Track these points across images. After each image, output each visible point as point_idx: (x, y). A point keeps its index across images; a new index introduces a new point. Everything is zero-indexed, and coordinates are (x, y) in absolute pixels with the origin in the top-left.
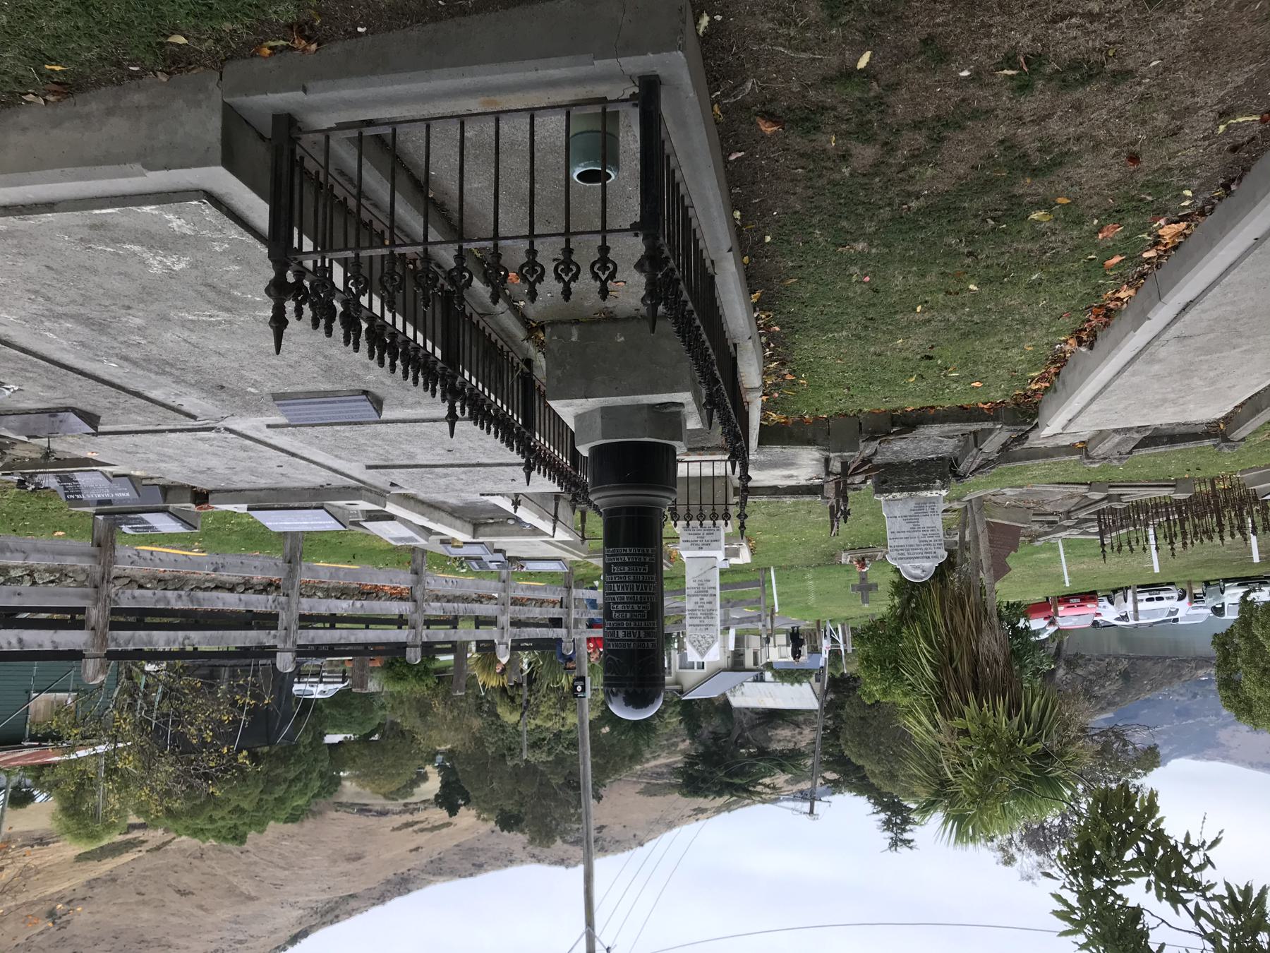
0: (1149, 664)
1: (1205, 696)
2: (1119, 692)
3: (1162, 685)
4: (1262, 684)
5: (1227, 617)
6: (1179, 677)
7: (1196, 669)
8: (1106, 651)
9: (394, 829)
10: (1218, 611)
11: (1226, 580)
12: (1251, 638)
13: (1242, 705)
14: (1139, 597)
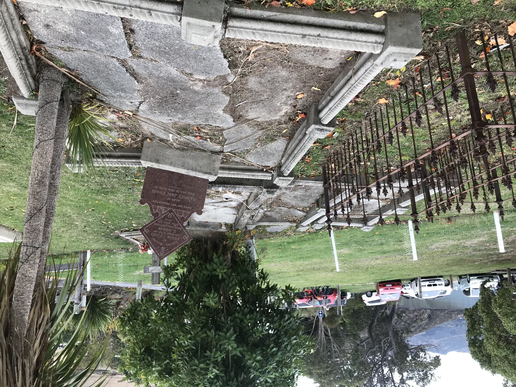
0: (439, 312)
1: (461, 326)
2: (427, 324)
3: (444, 321)
4: (499, 346)
5: (471, 296)
6: (451, 318)
7: (457, 315)
8: (422, 307)
9: (119, 381)
10: (467, 292)
11: (471, 275)
12: (490, 314)
13: (484, 358)
14: (423, 284)
